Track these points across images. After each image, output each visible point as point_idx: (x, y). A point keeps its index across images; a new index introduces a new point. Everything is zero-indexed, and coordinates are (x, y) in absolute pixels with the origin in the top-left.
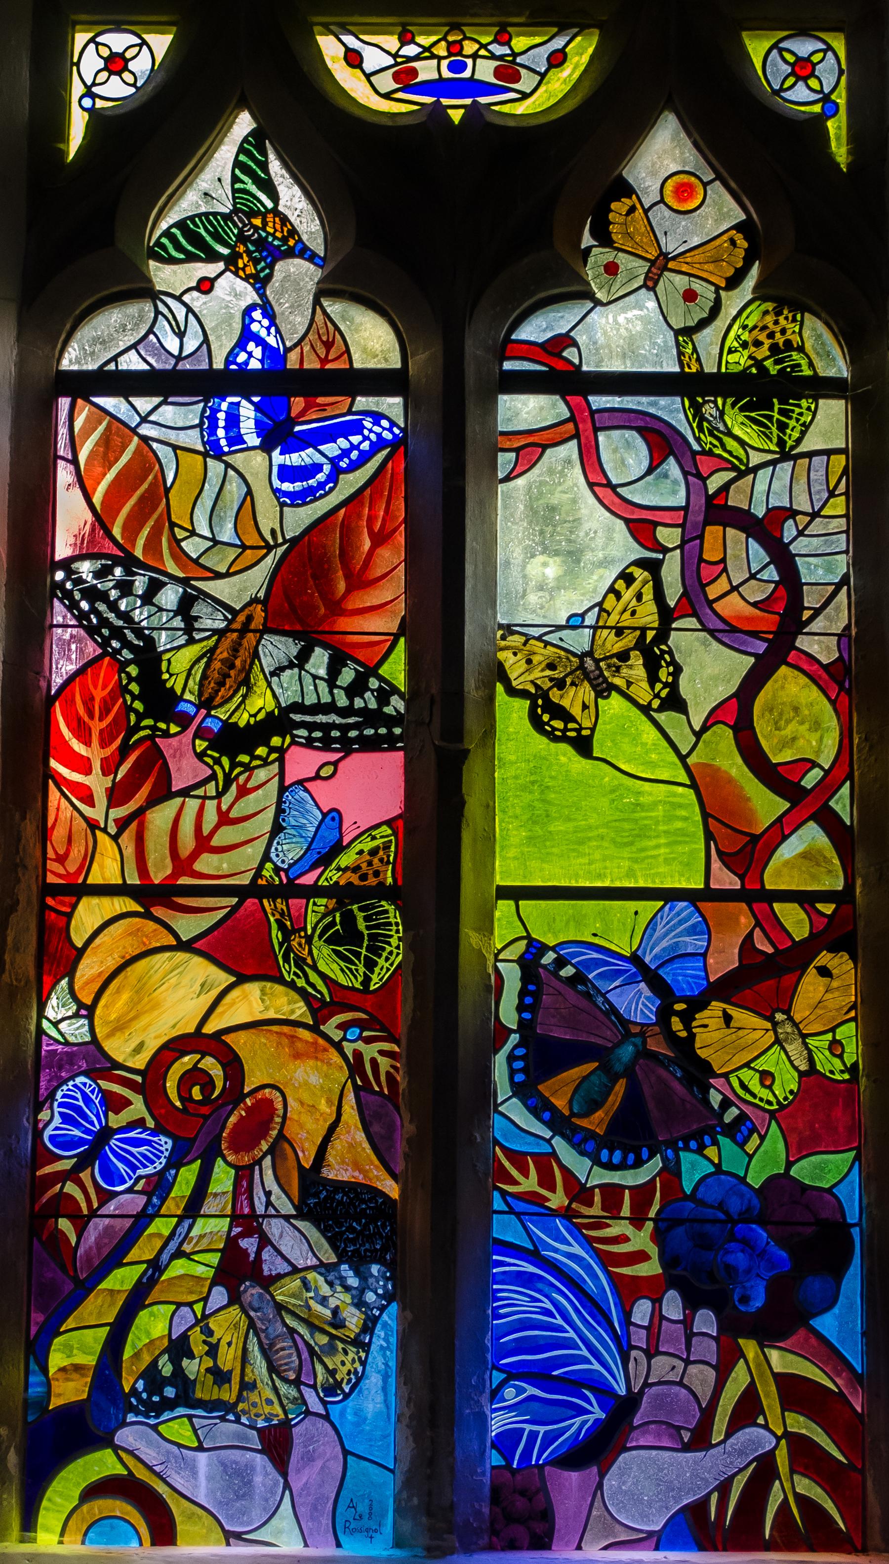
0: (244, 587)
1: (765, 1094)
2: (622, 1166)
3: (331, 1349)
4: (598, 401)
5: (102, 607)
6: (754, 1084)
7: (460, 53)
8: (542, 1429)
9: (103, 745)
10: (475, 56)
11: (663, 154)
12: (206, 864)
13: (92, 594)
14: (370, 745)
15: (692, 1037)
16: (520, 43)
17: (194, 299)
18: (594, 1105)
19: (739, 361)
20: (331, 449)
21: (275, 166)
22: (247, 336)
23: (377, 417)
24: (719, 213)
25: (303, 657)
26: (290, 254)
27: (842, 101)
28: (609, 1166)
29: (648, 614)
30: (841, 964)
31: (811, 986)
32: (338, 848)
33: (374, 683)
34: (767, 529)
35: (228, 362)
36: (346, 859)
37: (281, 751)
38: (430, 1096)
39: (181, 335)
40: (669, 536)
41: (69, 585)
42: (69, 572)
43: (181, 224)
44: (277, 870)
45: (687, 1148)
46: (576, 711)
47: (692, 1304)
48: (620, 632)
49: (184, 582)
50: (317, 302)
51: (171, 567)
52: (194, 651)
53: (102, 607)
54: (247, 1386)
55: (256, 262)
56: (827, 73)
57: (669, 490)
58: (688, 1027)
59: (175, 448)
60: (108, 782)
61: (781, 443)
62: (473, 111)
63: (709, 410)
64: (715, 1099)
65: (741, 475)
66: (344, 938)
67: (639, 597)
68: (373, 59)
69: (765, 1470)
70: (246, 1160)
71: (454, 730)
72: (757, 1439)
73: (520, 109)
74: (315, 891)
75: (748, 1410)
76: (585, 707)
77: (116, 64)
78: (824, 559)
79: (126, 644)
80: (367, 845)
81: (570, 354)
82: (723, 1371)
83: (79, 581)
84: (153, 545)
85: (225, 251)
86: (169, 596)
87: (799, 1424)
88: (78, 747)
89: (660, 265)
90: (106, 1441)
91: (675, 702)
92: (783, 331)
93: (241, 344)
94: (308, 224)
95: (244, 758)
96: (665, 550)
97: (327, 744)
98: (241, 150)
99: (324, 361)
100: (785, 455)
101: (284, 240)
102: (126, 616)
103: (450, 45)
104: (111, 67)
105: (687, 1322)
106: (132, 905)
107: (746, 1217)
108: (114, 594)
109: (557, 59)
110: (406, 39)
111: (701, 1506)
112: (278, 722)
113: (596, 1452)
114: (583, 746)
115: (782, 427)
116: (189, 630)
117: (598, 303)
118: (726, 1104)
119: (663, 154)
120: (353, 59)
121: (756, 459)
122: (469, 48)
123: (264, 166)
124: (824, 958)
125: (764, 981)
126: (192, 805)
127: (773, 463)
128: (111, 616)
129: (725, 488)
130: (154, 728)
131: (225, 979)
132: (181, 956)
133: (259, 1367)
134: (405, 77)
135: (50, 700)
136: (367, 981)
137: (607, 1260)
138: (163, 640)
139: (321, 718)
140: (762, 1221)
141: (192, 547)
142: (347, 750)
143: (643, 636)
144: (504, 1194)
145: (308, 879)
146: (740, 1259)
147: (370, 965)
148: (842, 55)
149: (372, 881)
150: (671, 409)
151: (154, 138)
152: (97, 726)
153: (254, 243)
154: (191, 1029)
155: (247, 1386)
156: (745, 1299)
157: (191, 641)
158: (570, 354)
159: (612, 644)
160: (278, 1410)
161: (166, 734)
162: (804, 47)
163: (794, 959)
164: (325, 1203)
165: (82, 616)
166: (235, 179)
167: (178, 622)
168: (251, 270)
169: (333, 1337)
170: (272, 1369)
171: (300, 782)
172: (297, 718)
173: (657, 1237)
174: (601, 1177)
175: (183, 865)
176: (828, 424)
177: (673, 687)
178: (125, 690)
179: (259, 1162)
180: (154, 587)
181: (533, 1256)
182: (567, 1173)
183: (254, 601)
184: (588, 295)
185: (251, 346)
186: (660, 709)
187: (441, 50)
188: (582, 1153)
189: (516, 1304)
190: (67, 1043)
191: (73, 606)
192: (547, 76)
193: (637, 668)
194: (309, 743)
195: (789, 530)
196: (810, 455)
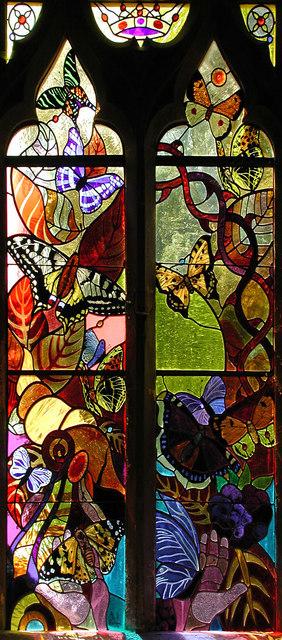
0: (72, 248)
1: (243, 452)
2: (198, 482)
3: (104, 554)
4: (189, 169)
5: (24, 257)
6: (241, 449)
7: (141, 15)
8: (172, 584)
9: (26, 313)
10: (147, 17)
11: (211, 61)
12: (61, 361)
13: (21, 251)
14: (115, 313)
15: (220, 431)
16: (163, 10)
17: (51, 124)
18: (188, 458)
19: (237, 152)
20: (99, 189)
21: (79, 67)
22: (70, 141)
23: (115, 175)
24: (229, 87)
25: (92, 276)
26: (84, 105)
27: (274, 36)
28: (193, 482)
29: (206, 259)
30: (268, 400)
31: (258, 410)
32: (104, 355)
33: (115, 288)
34: (246, 223)
35: (64, 152)
36: (107, 360)
37: (85, 316)
38: (135, 459)
39: (48, 140)
40: (213, 226)
41: (12, 247)
42: (13, 242)
43: (46, 92)
44: (84, 364)
45: (219, 475)
46: (182, 299)
47: (220, 535)
48: (197, 266)
49: (51, 246)
50: (94, 126)
51: (47, 240)
52: (56, 274)
53: (24, 257)
54: (78, 568)
55: (73, 108)
56: (270, 23)
57: (211, 207)
58: (219, 427)
59: (47, 189)
60: (27, 328)
61: (251, 186)
62: (147, 41)
63: (227, 172)
64: (228, 454)
65: (238, 200)
66: (107, 391)
67: (203, 251)
68: (112, 18)
69: (243, 599)
70: (76, 480)
71: (142, 308)
72: (243, 588)
73: (163, 40)
74: (96, 373)
75: (237, 578)
76: (185, 297)
77: (22, 20)
78: (265, 240)
79: (33, 272)
80: (114, 354)
81: (180, 148)
82: (231, 561)
83: (16, 246)
84: (40, 232)
85: (63, 104)
86: (46, 252)
87: (257, 584)
88: (17, 314)
89: (211, 110)
90: (33, 590)
91: (215, 295)
92: (252, 138)
93: (68, 144)
94: (92, 97)
95: (72, 319)
96: (212, 232)
97: (100, 312)
98: (67, 59)
99: (97, 152)
100: (253, 192)
101: (82, 99)
102: (31, 260)
103: (138, 11)
104: (22, 21)
105: (219, 543)
106: (38, 379)
107: (238, 501)
108: (28, 251)
109: (175, 18)
110: (123, 10)
111: (222, 615)
112: (83, 304)
113: (189, 593)
114: (185, 313)
115: (252, 179)
116: (53, 266)
117: (190, 126)
118: (231, 457)
119: (211, 61)
120: (105, 18)
121: (243, 193)
122: (145, 13)
123: (74, 66)
124: (264, 399)
125: (243, 409)
126: (56, 337)
127: (248, 195)
128: (27, 260)
129: (232, 206)
130: (42, 307)
131: (68, 408)
132: (53, 399)
133: (81, 561)
134: (123, 26)
135: (8, 294)
136: (114, 408)
137: (193, 518)
138: (45, 270)
139: (98, 302)
140: (243, 503)
141: (53, 231)
142: (107, 316)
143: (204, 268)
144: (160, 492)
145: (94, 368)
146: (236, 519)
147: (115, 402)
148: (275, 14)
149: (116, 369)
150: (214, 172)
151: (37, 52)
152: (23, 306)
153: (72, 100)
154: (57, 428)
155: (78, 568)
156: (237, 534)
157: (54, 271)
158: (180, 148)
159: (194, 271)
160: (88, 577)
161: (46, 309)
162: (261, 11)
163: (254, 399)
164: (104, 497)
165: (17, 260)
166: (65, 72)
167: (49, 263)
168: (71, 113)
169: (105, 549)
170: (86, 561)
171: (92, 329)
172: (90, 302)
173: (209, 509)
174: (191, 486)
175: (53, 362)
176: (267, 179)
177: (215, 288)
178: (34, 299)
179: (80, 481)
180: (41, 247)
181: (169, 517)
182: (180, 485)
183: (75, 253)
184: (186, 123)
185: (72, 145)
186: (210, 298)
187: (135, 14)
188: (184, 476)
189: (163, 535)
190: (16, 548)
191: (14, 256)
192: (170, 25)
193: (202, 282)
194: (94, 313)
195: (254, 222)
196: (260, 191)
